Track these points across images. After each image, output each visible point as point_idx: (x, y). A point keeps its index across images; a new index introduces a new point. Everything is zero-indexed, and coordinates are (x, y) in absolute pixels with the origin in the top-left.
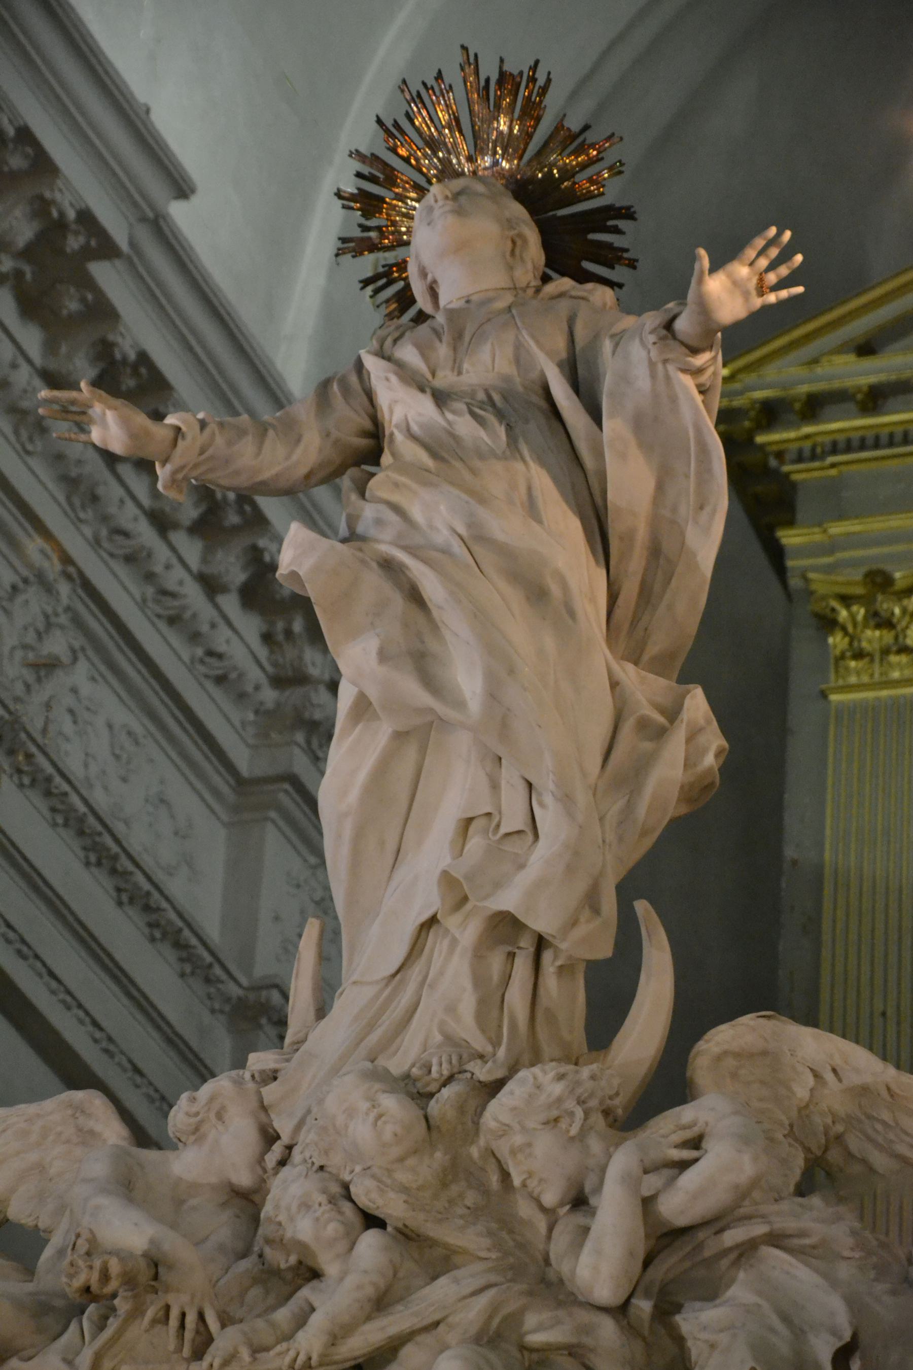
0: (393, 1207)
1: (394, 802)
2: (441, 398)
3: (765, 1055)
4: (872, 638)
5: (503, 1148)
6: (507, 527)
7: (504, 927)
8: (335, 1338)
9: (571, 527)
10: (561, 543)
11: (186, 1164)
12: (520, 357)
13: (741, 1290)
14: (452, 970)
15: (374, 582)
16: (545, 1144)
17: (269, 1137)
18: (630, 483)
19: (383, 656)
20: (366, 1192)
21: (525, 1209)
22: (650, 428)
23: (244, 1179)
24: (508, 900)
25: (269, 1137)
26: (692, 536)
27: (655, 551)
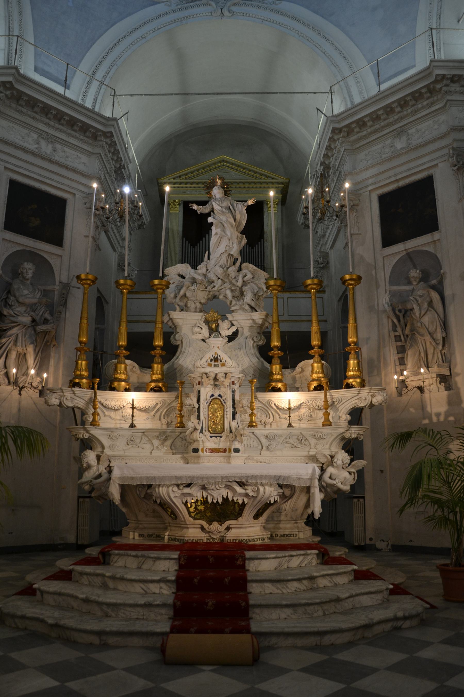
0: (221, 277)
1: (219, 243)
2: (221, 207)
3: (247, 266)
4: (174, 206)
5: (229, 273)
6: (230, 220)
7: (230, 255)
8: (218, 288)
9: (233, 220)
10: (232, 220)
11: (199, 271)
12: (227, 204)
13: (249, 286)
14: (224, 258)
15: (220, 224)
16: (233, 273)
17: (207, 270)
18: (238, 217)
19: (221, 231)
20: (219, 276)
21: (230, 278)
22: (241, 212)
23: (205, 273)
24: (232, 253)
25: (207, 270)
26: (243, 222)
27: (239, 223)
